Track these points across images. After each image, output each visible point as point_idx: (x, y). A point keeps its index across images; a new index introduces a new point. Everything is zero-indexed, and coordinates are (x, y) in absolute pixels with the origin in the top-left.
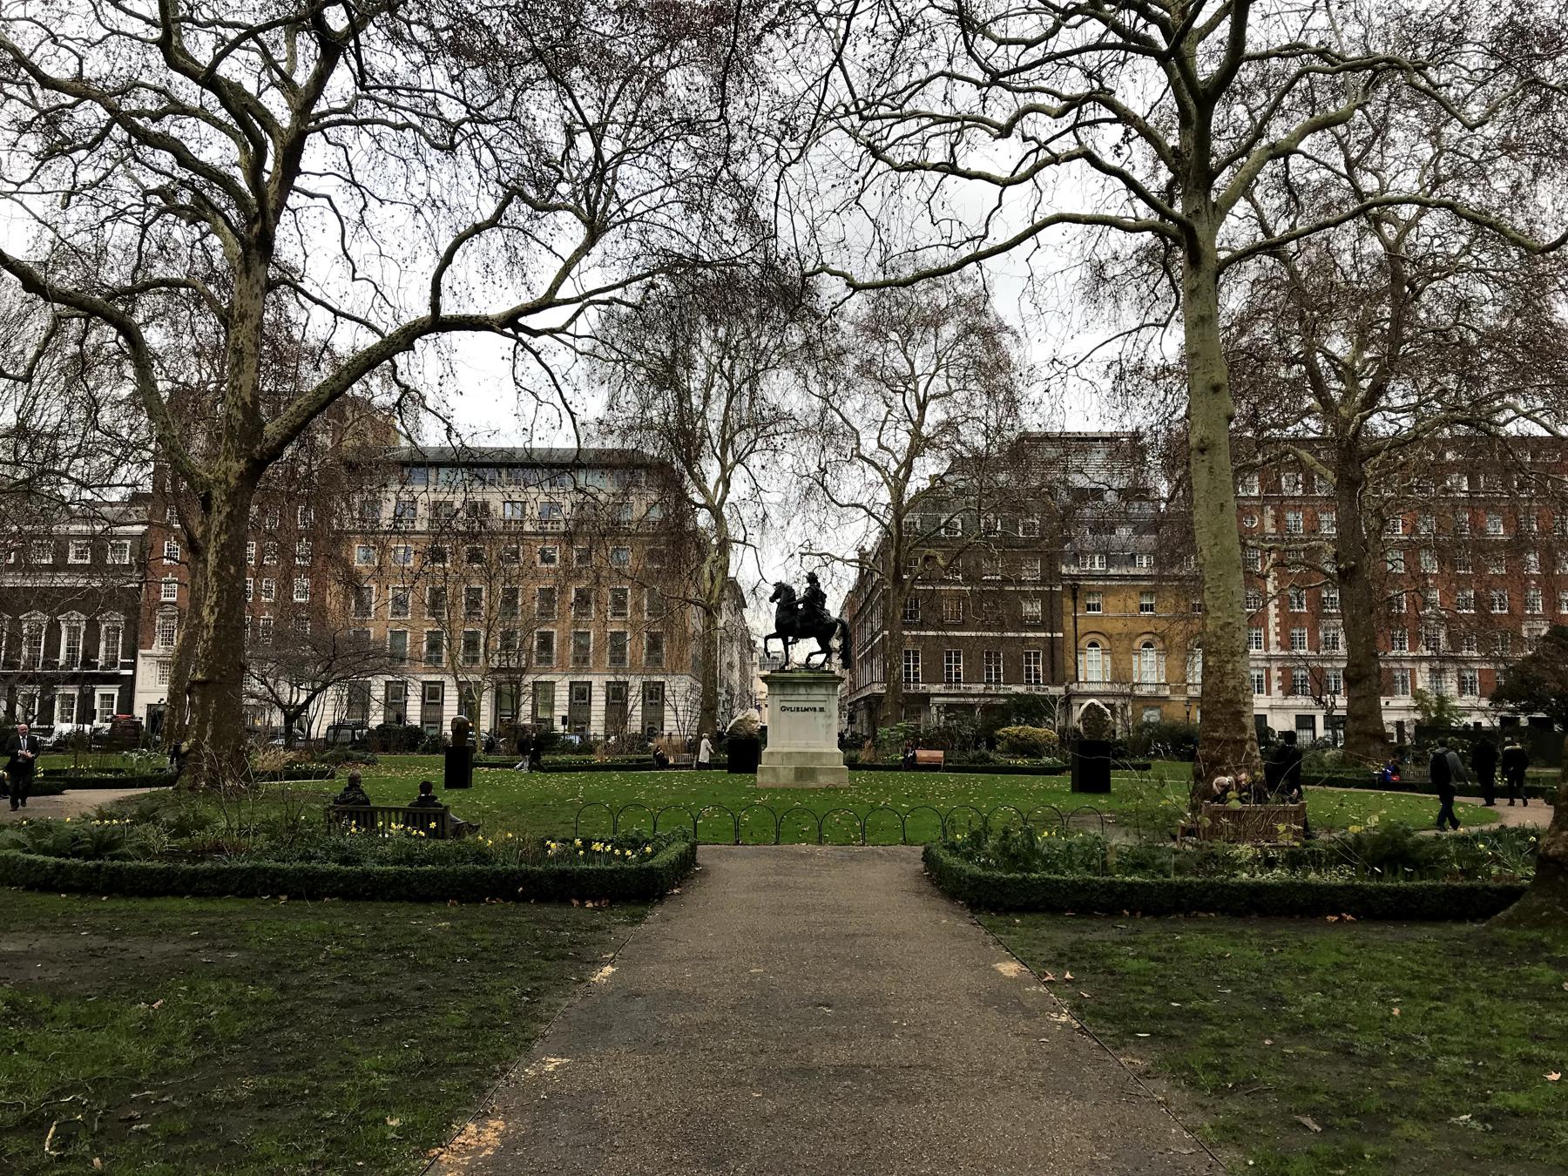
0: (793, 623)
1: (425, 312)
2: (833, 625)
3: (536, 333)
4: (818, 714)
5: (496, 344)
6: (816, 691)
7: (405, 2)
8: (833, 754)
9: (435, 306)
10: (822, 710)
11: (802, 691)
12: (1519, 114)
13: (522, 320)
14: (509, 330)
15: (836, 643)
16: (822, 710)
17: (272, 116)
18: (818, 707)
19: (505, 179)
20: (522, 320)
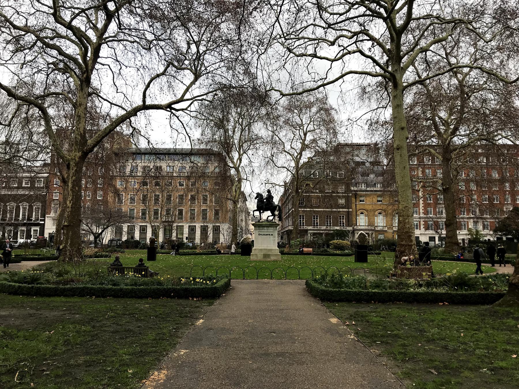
0: (263, 206)
1: (141, 103)
2: (276, 207)
3: (177, 110)
4: (271, 236)
5: (164, 114)
6: (270, 228)
8: (276, 250)
9: (144, 101)
10: (272, 235)
11: (266, 228)
13: (173, 106)
14: (168, 109)
15: (277, 213)
16: (272, 235)
17: (90, 38)
18: (271, 234)
20: (173, 106)
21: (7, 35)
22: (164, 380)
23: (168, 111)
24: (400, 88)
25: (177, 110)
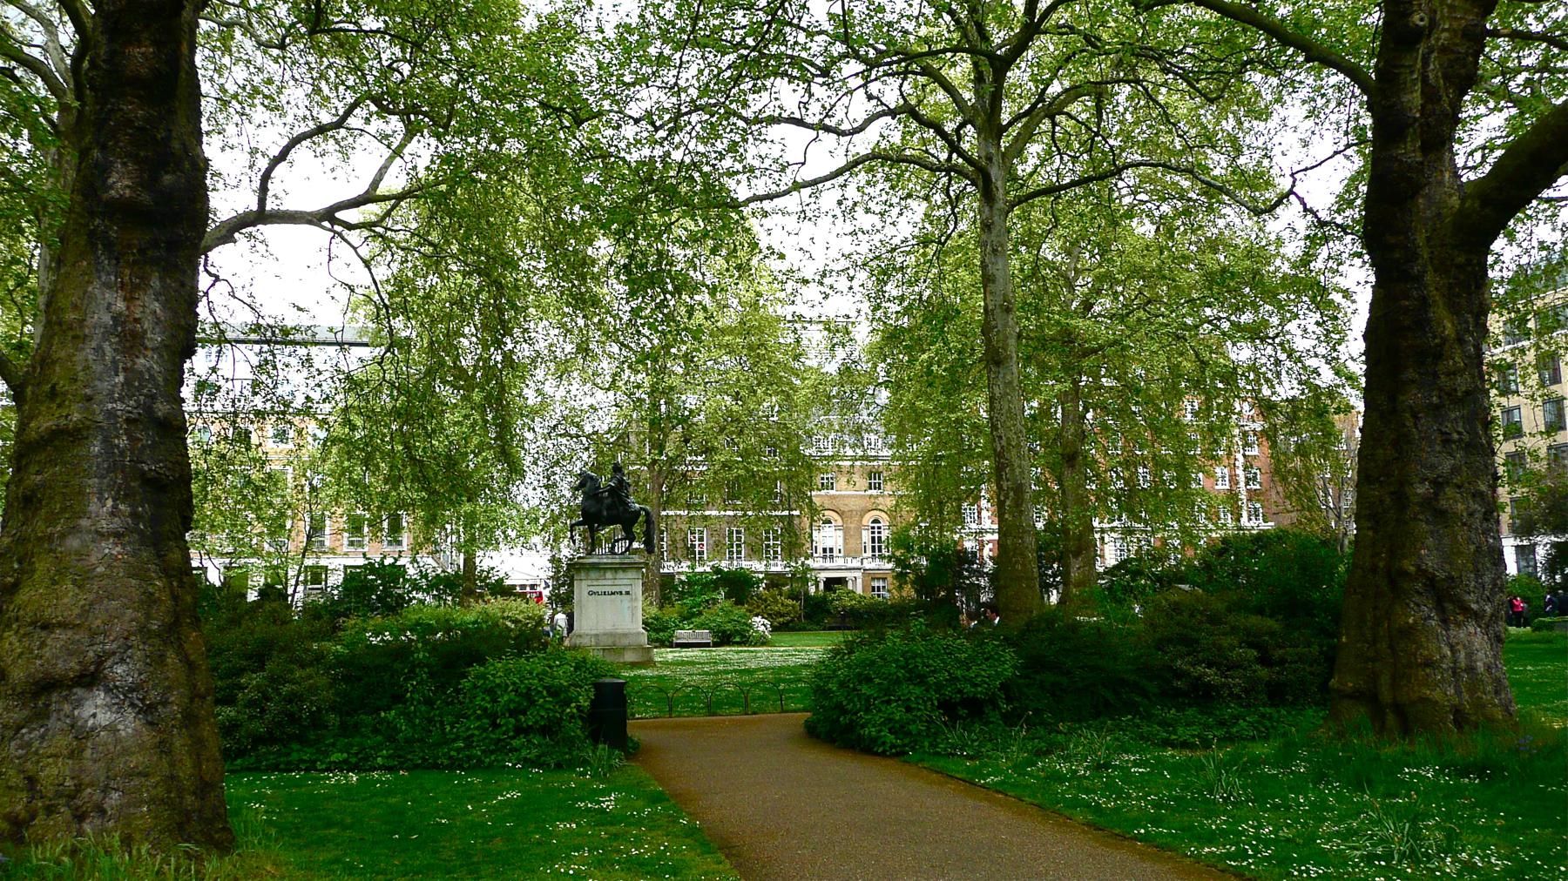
0: (600, 512)
1: (255, 207)
2: (637, 514)
3: (350, 227)
4: (624, 597)
5: (317, 236)
6: (621, 575)
7: (58, 877)
8: (639, 633)
9: (262, 202)
10: (628, 593)
11: (609, 575)
12: (302, 61)
13: (339, 215)
14: (326, 224)
15: (637, 529)
16: (628, 593)
17: (1372, 305)
18: (624, 589)
19: (775, 264)
20: (339, 215)
21: (906, 83)
22: (233, 588)
23: (324, 228)
24: (1000, 205)
25: (350, 227)
